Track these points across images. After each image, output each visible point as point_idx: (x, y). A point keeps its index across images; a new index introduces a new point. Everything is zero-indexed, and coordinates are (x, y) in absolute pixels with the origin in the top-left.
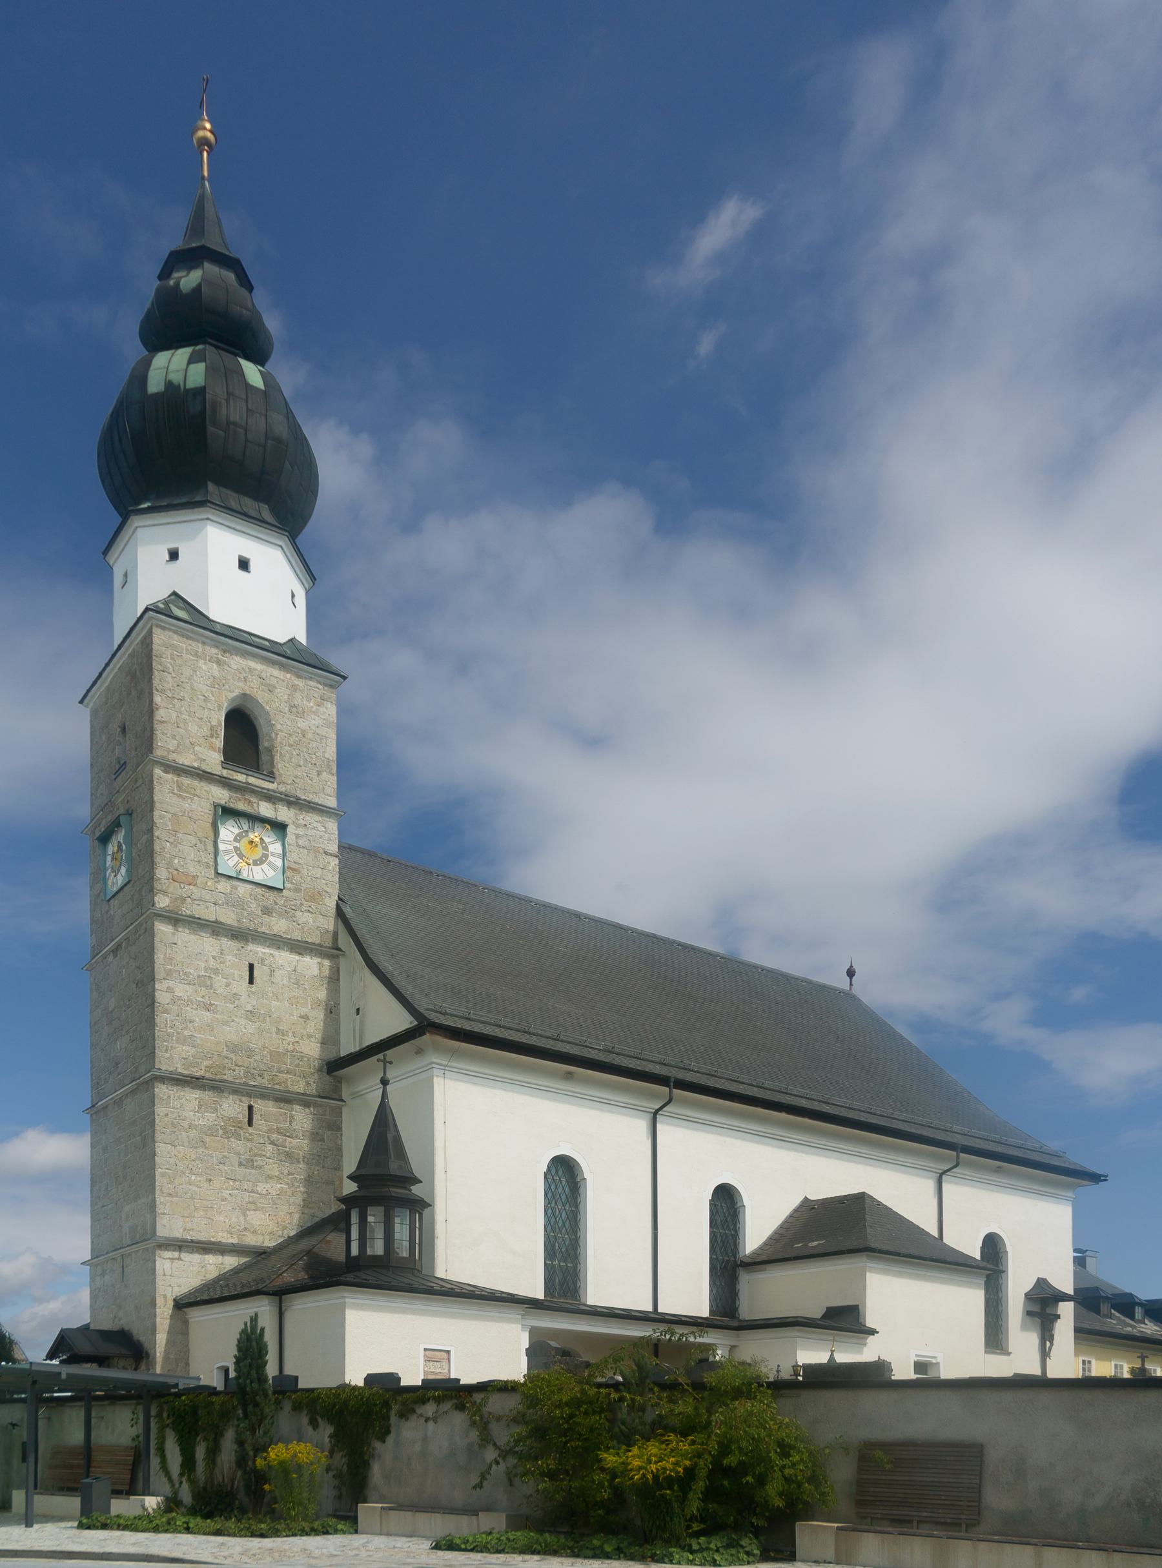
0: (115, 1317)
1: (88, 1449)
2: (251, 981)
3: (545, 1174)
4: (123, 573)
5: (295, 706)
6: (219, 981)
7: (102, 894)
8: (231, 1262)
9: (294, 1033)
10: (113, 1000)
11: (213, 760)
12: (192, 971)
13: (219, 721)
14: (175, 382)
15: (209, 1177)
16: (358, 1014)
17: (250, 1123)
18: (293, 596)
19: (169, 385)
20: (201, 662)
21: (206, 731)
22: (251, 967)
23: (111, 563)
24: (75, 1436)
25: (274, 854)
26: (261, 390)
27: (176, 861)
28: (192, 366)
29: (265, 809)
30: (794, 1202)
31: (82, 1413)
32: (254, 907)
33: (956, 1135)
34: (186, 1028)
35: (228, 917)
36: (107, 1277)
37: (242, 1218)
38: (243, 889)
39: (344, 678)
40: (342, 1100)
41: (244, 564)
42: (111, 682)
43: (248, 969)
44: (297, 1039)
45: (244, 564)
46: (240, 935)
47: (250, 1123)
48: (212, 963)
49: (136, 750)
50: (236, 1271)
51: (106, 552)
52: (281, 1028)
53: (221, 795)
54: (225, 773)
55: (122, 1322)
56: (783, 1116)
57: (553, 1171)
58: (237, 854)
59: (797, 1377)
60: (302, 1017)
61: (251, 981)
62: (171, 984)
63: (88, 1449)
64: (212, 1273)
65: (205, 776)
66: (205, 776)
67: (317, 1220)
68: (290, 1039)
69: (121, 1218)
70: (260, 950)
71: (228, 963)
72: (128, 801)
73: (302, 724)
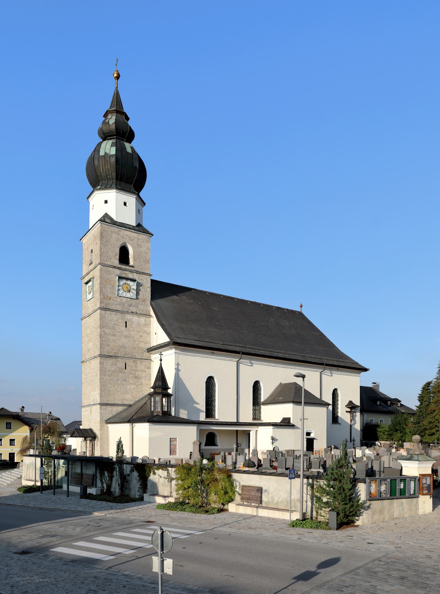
0: (89, 424)
1: (82, 474)
2: (126, 327)
3: (206, 382)
4: (91, 250)
5: (139, 245)
6: (117, 327)
7: (86, 299)
8: (120, 409)
9: (138, 341)
10: (88, 331)
11: (116, 262)
12: (110, 325)
13: (118, 251)
14: (107, 152)
15: (114, 385)
16: (156, 334)
17: (126, 369)
18: (139, 210)
19: (106, 153)
20: (113, 234)
21: (114, 254)
22: (126, 322)
23: (89, 201)
24: (78, 470)
25: (133, 289)
26: (131, 153)
27: (106, 293)
28: (112, 148)
29: (130, 276)
30: (277, 384)
31: (80, 464)
32: (126, 305)
33: (34, 527)
34: (108, 342)
35: (119, 308)
36: (87, 412)
37: (123, 396)
38: (124, 300)
39: (153, 235)
40: (151, 360)
41: (125, 204)
42: (89, 237)
43: (125, 323)
44: (139, 343)
45: (125, 204)
46: (122, 312)
47: (126, 369)
48: (116, 322)
49: (95, 259)
50: (121, 412)
51: (88, 198)
52: (134, 340)
53: (118, 272)
54: (120, 266)
55: (91, 426)
56: (274, 360)
57: (208, 381)
58: (123, 290)
59: (351, 410)
60: (140, 336)
61: (126, 327)
62: (104, 329)
63: (82, 474)
64: (114, 413)
65: (115, 267)
66: (115, 267)
67: (144, 395)
68: (137, 343)
69: (90, 396)
70: (128, 317)
71: (120, 322)
72: (93, 274)
73: (141, 250)
